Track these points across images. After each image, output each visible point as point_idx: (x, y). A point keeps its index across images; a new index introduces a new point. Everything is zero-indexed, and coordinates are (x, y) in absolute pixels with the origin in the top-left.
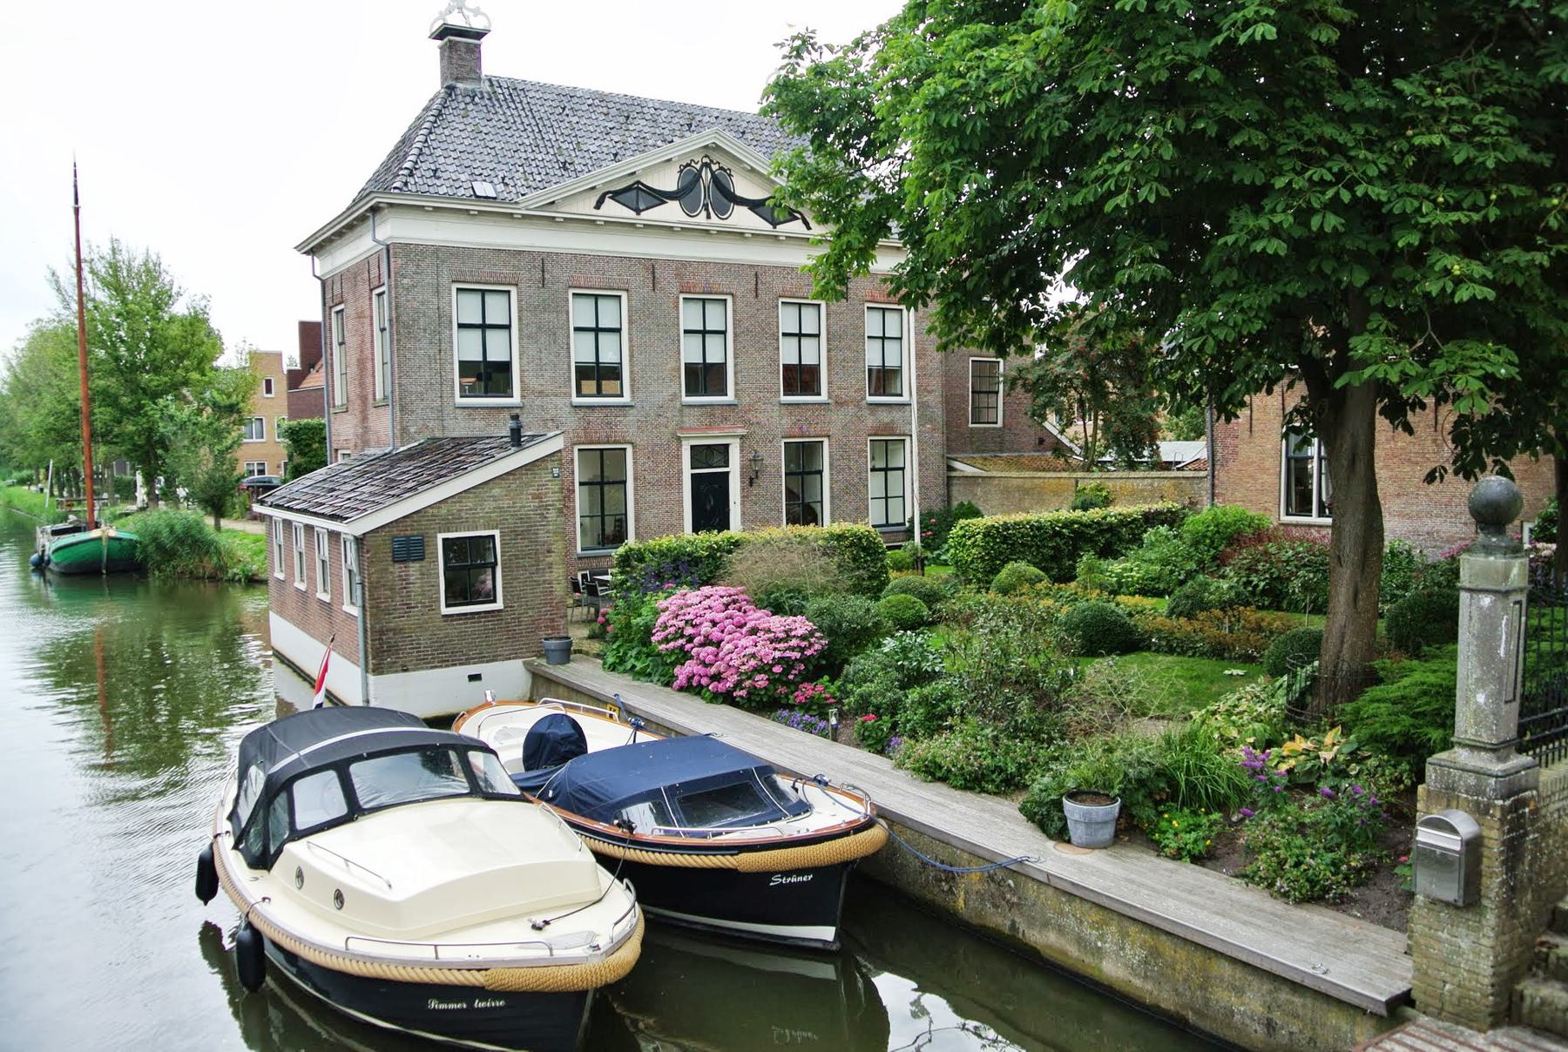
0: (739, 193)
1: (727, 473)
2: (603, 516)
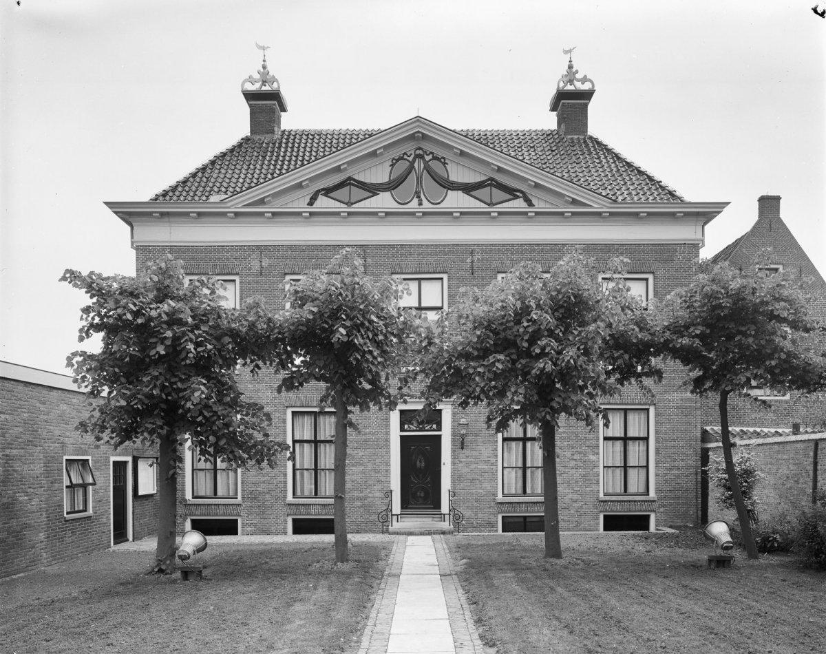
0: (453, 178)
1: (440, 436)
2: (625, 467)
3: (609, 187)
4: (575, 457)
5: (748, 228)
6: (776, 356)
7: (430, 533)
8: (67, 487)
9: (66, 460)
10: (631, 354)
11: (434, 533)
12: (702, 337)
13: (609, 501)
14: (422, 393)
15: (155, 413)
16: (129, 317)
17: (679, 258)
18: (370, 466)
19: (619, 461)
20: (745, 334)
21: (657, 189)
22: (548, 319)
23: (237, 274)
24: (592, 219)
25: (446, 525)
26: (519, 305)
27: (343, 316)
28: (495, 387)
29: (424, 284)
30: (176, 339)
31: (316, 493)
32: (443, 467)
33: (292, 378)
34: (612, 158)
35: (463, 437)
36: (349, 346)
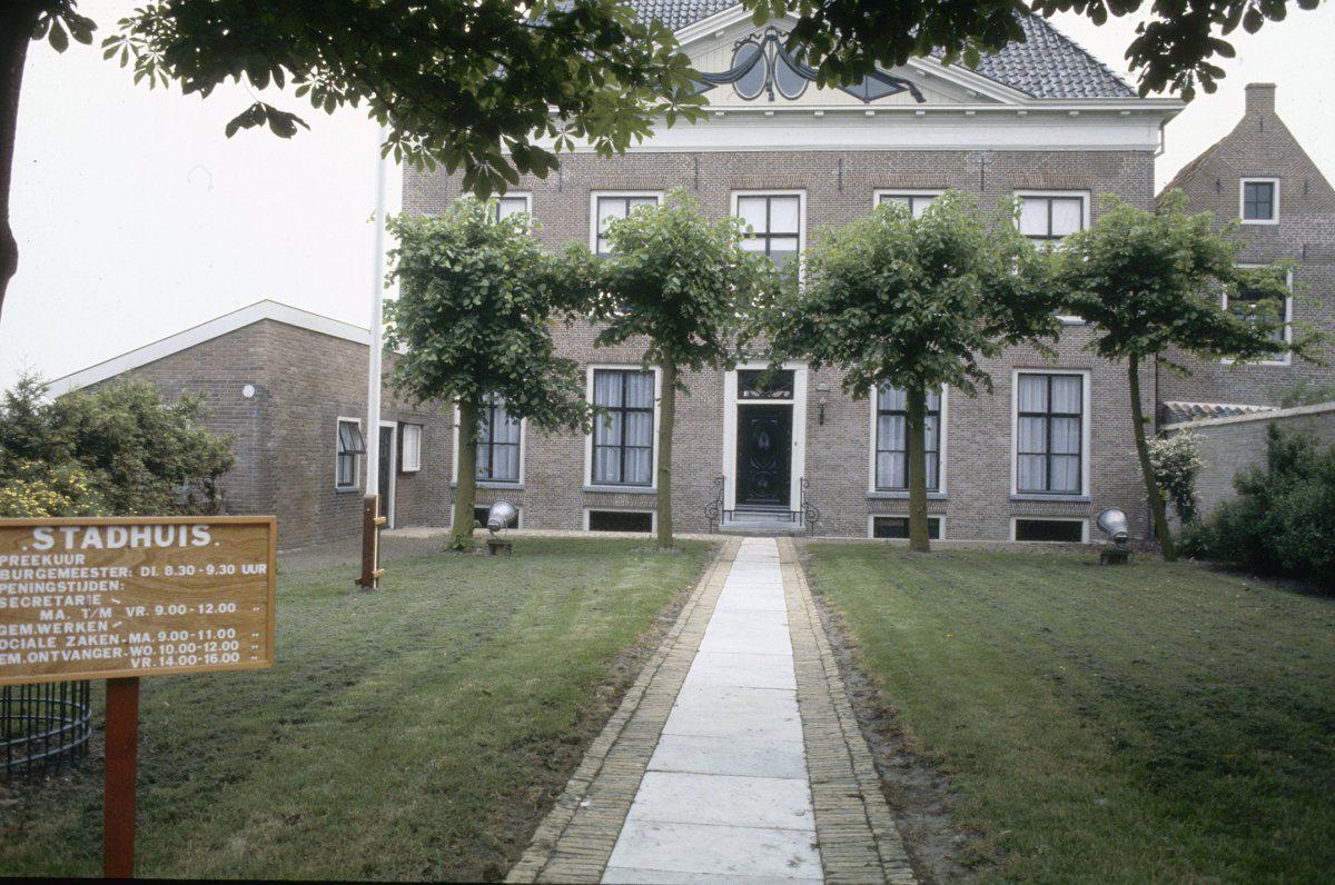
2: (1049, 455)
3: (1032, 73)
4: (978, 438)
5: (1228, 130)
6: (1186, 316)
8: (340, 454)
9: (341, 422)
10: (1024, 311)
11: (780, 535)
12: (1099, 289)
13: (1024, 501)
14: (766, 351)
15: (465, 368)
16: (448, 264)
17: (1125, 170)
18: (695, 444)
19: (1040, 447)
20: (1148, 287)
21: (1098, 75)
22: (910, 270)
23: (530, 190)
24: (1001, 118)
25: (796, 526)
27: (678, 264)
28: (850, 347)
29: (1057, 206)
30: (493, 289)
31: (622, 480)
34: (1041, 29)
36: (683, 297)
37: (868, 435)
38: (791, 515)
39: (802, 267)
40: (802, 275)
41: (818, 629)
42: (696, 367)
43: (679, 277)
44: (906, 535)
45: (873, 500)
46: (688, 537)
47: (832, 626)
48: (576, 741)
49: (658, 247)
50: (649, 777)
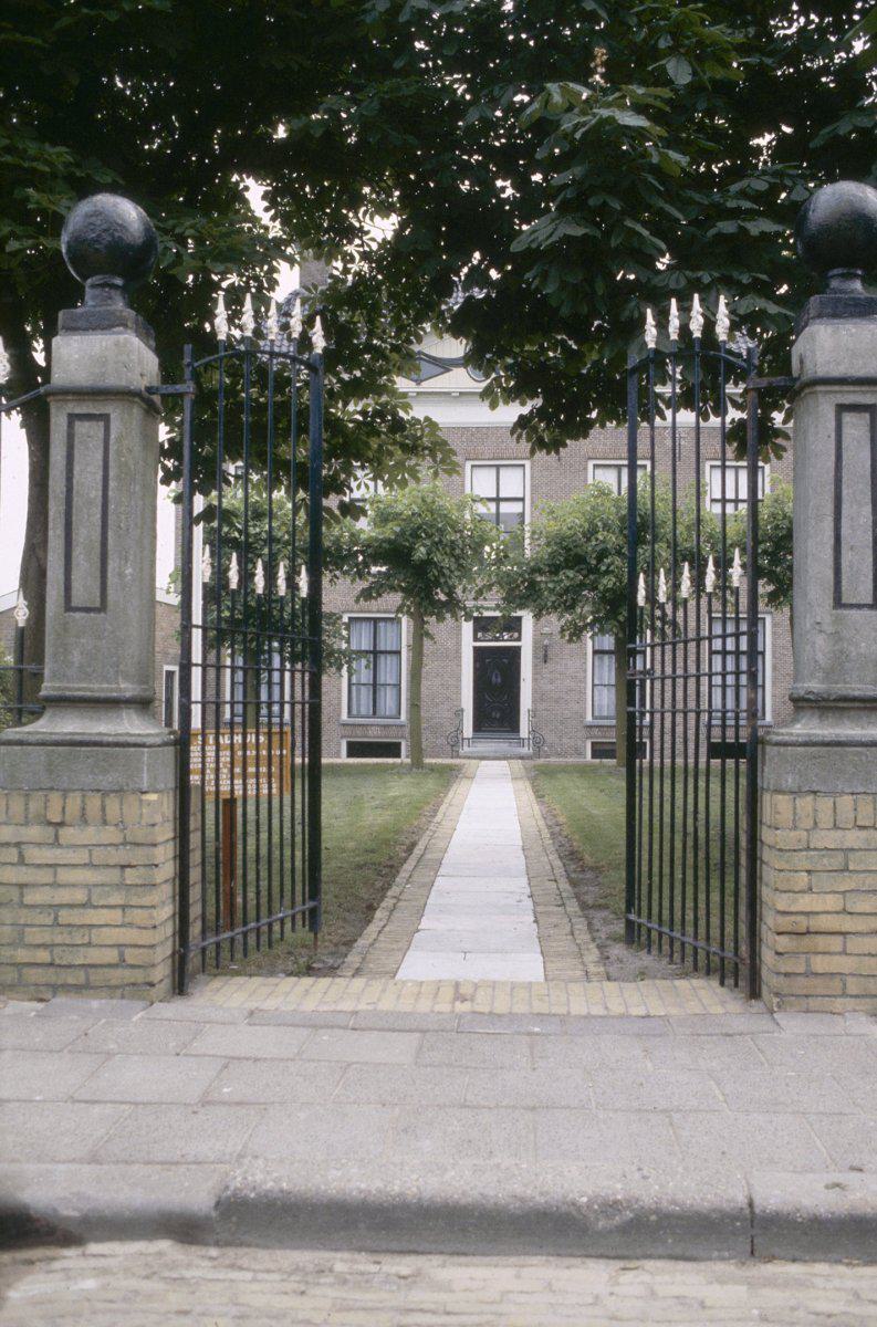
1: (519, 648)
7: (505, 758)
11: (511, 758)
22: (613, 539)
25: (525, 750)
26: (586, 525)
31: (374, 712)
32: (522, 684)
33: (370, 588)
35: (546, 648)
36: (428, 562)
37: (585, 671)
38: (521, 742)
39: (527, 535)
40: (527, 541)
41: (539, 817)
42: (441, 618)
43: (424, 545)
44: (613, 757)
45: (591, 727)
46: (434, 761)
47: (549, 815)
48: (392, 867)
49: (408, 520)
50: (438, 879)
